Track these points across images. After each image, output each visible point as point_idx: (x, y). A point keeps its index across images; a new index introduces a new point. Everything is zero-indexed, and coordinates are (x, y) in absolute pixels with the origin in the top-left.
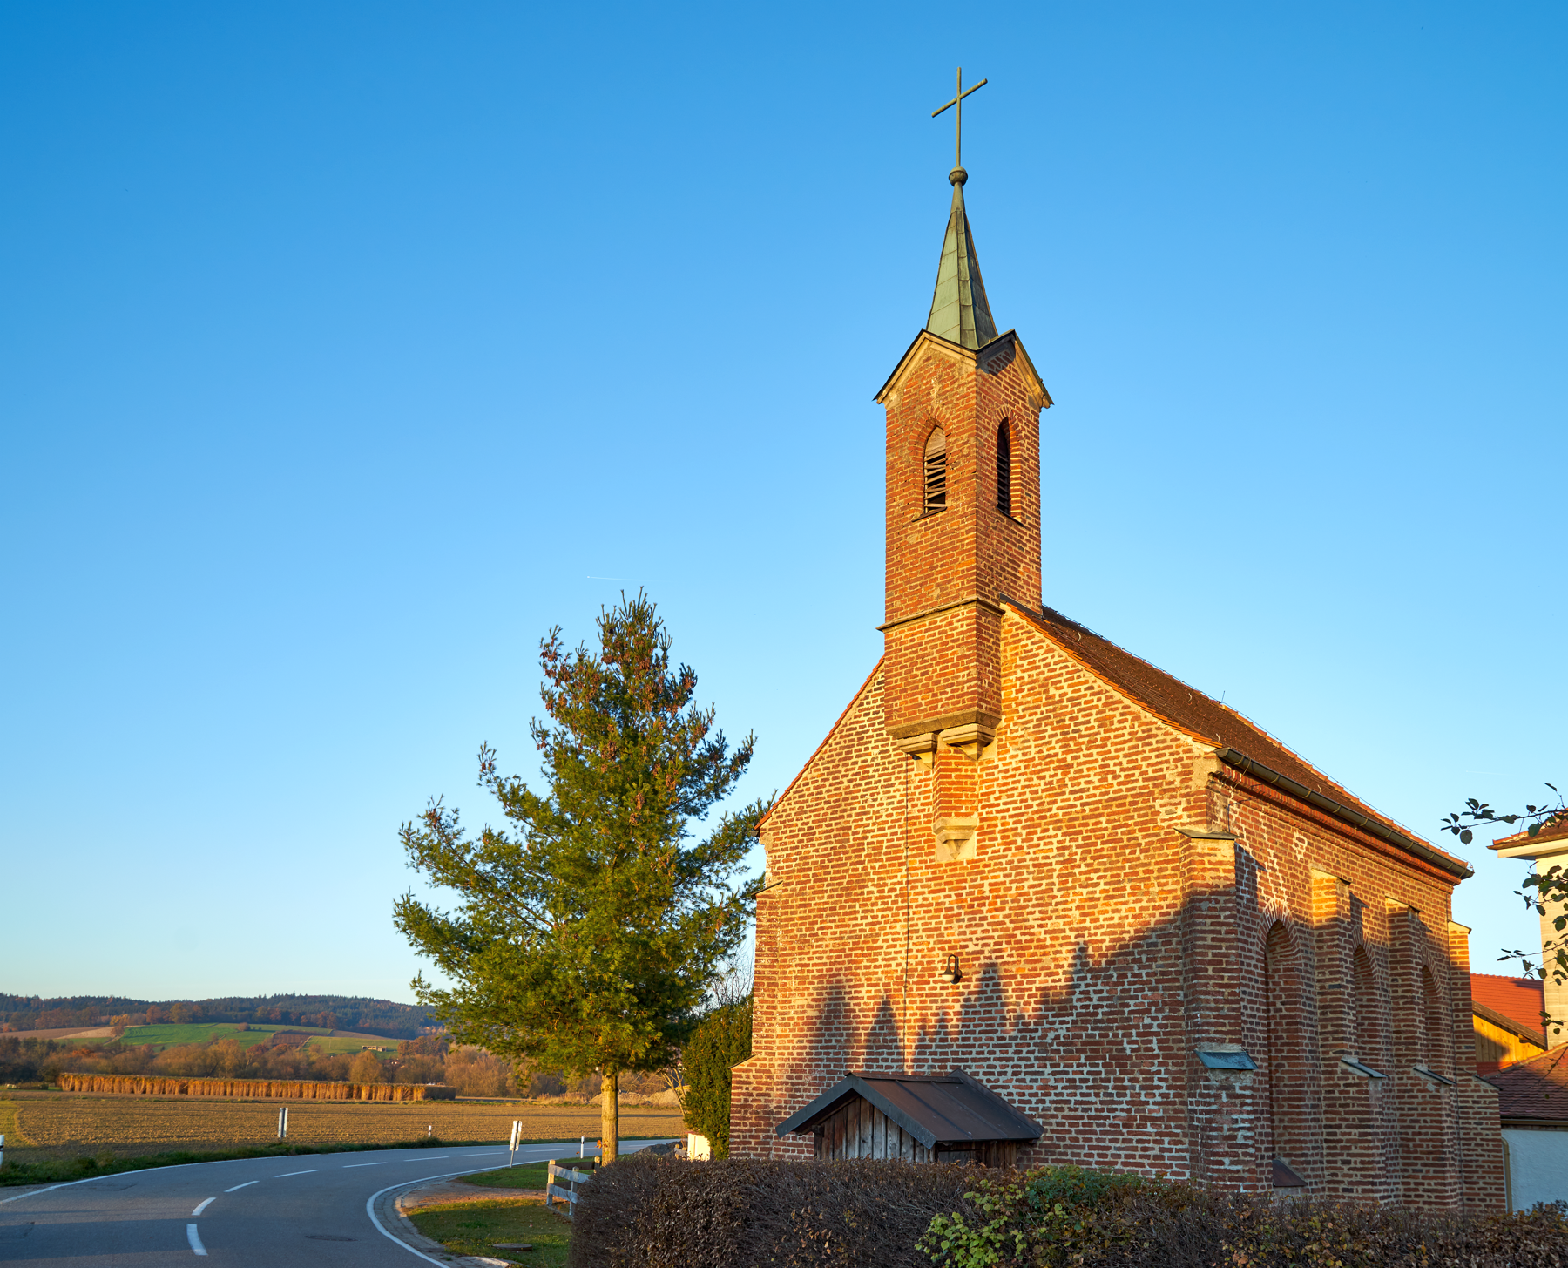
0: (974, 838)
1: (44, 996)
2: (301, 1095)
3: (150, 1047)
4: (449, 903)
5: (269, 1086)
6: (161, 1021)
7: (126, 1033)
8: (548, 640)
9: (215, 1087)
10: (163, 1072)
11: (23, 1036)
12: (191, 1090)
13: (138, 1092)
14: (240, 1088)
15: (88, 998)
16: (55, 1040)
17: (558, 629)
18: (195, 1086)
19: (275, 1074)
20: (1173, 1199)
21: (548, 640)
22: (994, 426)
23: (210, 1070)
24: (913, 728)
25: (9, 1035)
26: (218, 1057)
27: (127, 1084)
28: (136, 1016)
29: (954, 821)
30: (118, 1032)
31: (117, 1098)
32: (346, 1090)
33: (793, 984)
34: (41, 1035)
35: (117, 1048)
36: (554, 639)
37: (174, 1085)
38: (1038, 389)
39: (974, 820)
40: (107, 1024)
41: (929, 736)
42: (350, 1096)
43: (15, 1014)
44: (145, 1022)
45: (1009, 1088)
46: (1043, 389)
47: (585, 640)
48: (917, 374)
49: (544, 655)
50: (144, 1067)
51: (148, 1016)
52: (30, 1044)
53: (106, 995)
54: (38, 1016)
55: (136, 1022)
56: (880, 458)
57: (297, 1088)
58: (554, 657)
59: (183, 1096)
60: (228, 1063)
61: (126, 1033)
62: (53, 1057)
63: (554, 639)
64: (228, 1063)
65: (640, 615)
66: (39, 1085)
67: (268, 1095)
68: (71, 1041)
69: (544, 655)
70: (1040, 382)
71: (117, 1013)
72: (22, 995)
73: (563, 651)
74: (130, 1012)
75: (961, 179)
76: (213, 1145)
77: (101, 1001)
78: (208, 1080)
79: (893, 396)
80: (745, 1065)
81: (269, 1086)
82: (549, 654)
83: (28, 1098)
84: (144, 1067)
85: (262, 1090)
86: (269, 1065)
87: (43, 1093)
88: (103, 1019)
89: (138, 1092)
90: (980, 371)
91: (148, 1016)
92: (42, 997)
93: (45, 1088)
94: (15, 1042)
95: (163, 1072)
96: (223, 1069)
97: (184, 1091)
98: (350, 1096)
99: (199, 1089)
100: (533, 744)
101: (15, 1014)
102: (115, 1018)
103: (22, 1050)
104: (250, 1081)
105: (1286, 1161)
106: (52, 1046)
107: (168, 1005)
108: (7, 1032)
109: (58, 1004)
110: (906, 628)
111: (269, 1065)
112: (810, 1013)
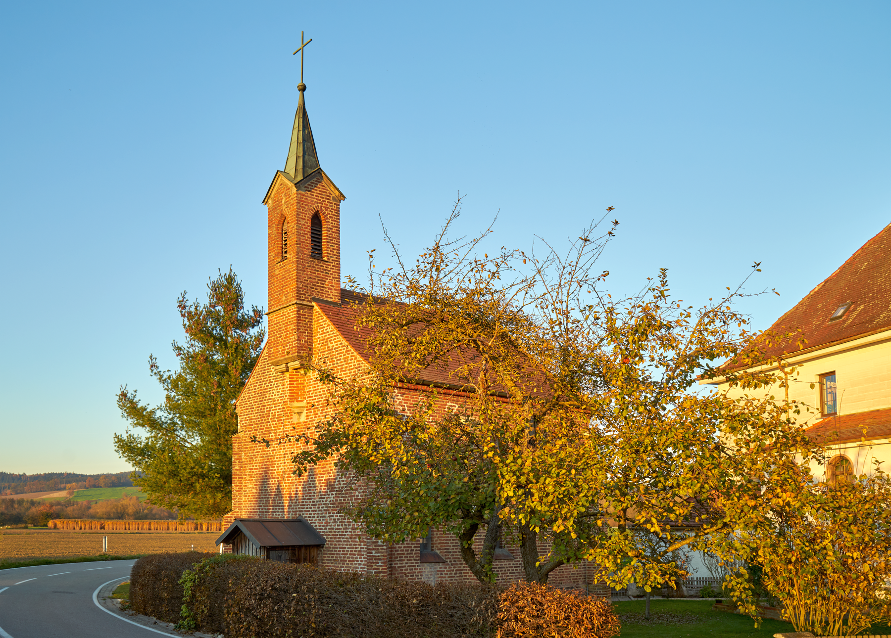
0: (305, 412)
1: (29, 473)
2: (168, 529)
3: (89, 502)
4: (143, 434)
5: (150, 524)
6: (94, 486)
7: (75, 494)
8: (181, 299)
9: (120, 525)
10: (93, 517)
11: (16, 497)
12: (106, 527)
13: (77, 529)
14: (134, 525)
15: (53, 474)
16: (35, 500)
17: (185, 293)
18: (108, 524)
19: (157, 516)
20: (705, 580)
21: (181, 299)
22: (309, 215)
23: (120, 515)
24: (278, 362)
25: (8, 497)
26: (125, 507)
27: (71, 525)
28: (80, 483)
29: (296, 404)
30: (71, 494)
31: (65, 533)
32: (194, 525)
33: (248, 478)
34: (27, 497)
35: (69, 503)
36: (184, 298)
37: (96, 524)
38: (337, 193)
39: (304, 404)
40: (64, 489)
41: (284, 365)
42: (196, 529)
43: (13, 484)
44: (85, 487)
45: (316, 524)
46: (340, 192)
47: (201, 298)
48: (278, 192)
49: (179, 306)
50: (85, 514)
51: (87, 483)
52: (20, 502)
53: (63, 471)
54: (26, 485)
55: (81, 488)
56: (265, 231)
57: (165, 525)
58: (184, 308)
59: (103, 531)
60: (131, 510)
61: (75, 494)
62: (34, 510)
63: (184, 298)
64: (131, 510)
65: (231, 279)
66: (23, 525)
67: (150, 529)
68: (43, 500)
69: (179, 306)
70: (337, 189)
71: (70, 482)
72: (16, 473)
73: (188, 304)
74: (77, 481)
75: (303, 89)
76: (25, 559)
77: (60, 475)
78: (115, 521)
79: (270, 201)
80: (229, 514)
81: (150, 524)
82: (182, 306)
83: (16, 533)
84: (85, 514)
85: (146, 526)
86: (154, 512)
87: (25, 530)
88: (62, 486)
89: (77, 529)
90: (300, 192)
91: (87, 483)
92: (28, 474)
93: (26, 528)
94: (12, 501)
95: (93, 517)
96: (128, 515)
97: (102, 528)
98: (196, 529)
99: (111, 526)
100: (174, 354)
101: (13, 484)
102: (68, 485)
103: (16, 506)
104: (139, 521)
105: (438, 552)
106: (33, 503)
107: (98, 476)
108: (9, 495)
109: (36, 477)
110: (274, 314)
111: (154, 512)
112: (254, 491)
